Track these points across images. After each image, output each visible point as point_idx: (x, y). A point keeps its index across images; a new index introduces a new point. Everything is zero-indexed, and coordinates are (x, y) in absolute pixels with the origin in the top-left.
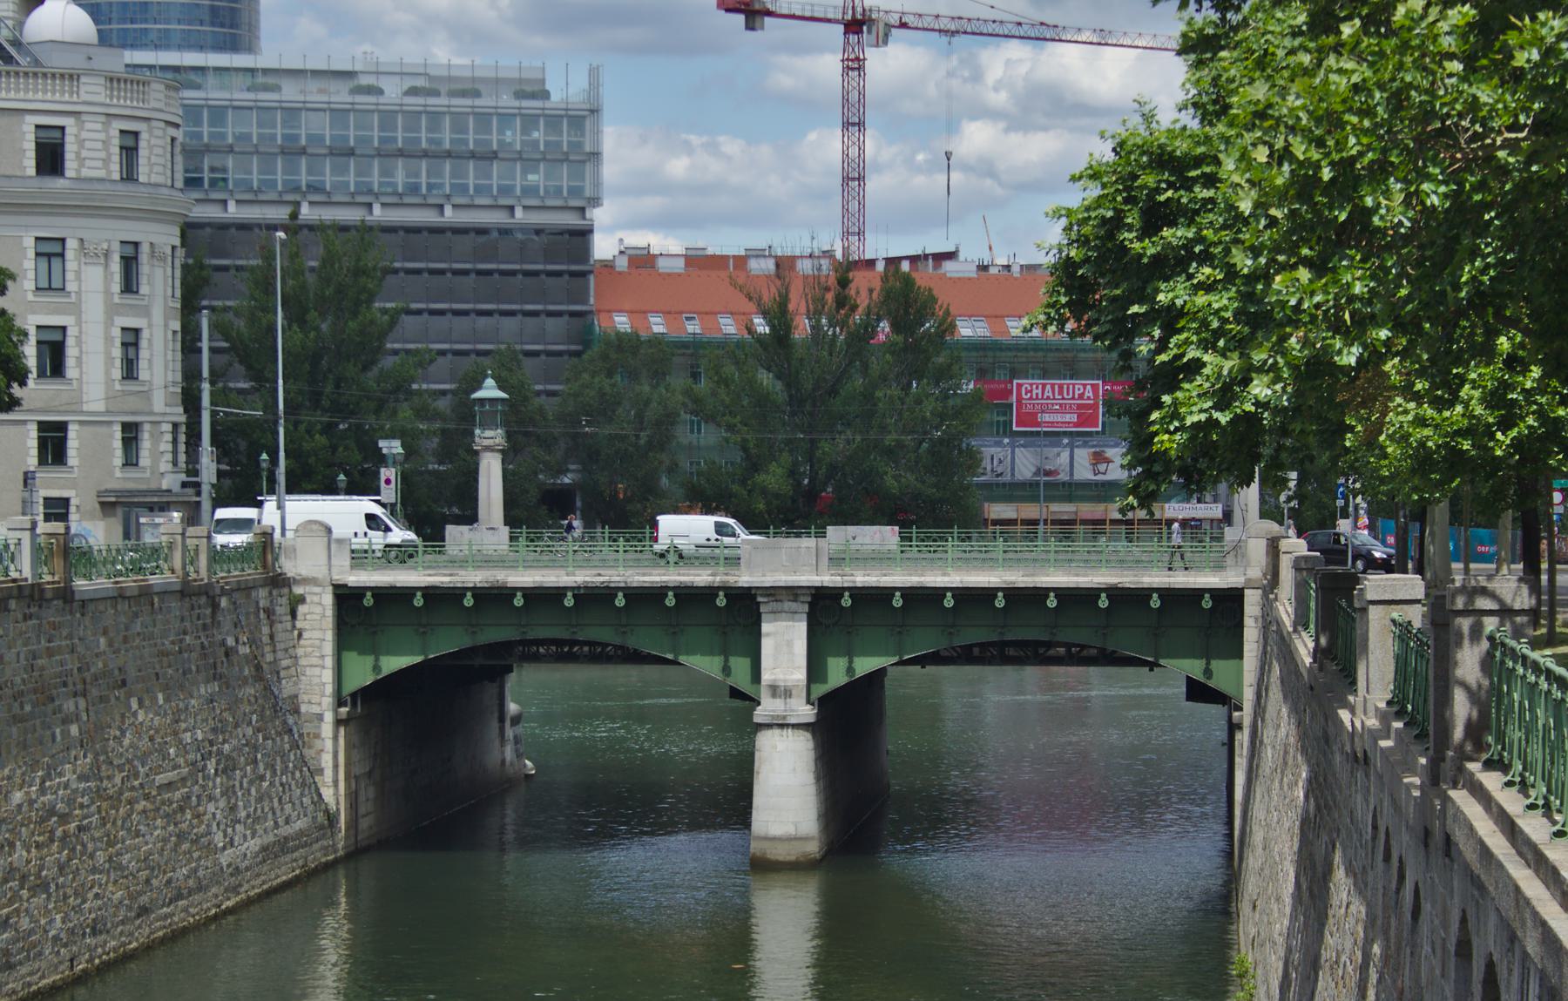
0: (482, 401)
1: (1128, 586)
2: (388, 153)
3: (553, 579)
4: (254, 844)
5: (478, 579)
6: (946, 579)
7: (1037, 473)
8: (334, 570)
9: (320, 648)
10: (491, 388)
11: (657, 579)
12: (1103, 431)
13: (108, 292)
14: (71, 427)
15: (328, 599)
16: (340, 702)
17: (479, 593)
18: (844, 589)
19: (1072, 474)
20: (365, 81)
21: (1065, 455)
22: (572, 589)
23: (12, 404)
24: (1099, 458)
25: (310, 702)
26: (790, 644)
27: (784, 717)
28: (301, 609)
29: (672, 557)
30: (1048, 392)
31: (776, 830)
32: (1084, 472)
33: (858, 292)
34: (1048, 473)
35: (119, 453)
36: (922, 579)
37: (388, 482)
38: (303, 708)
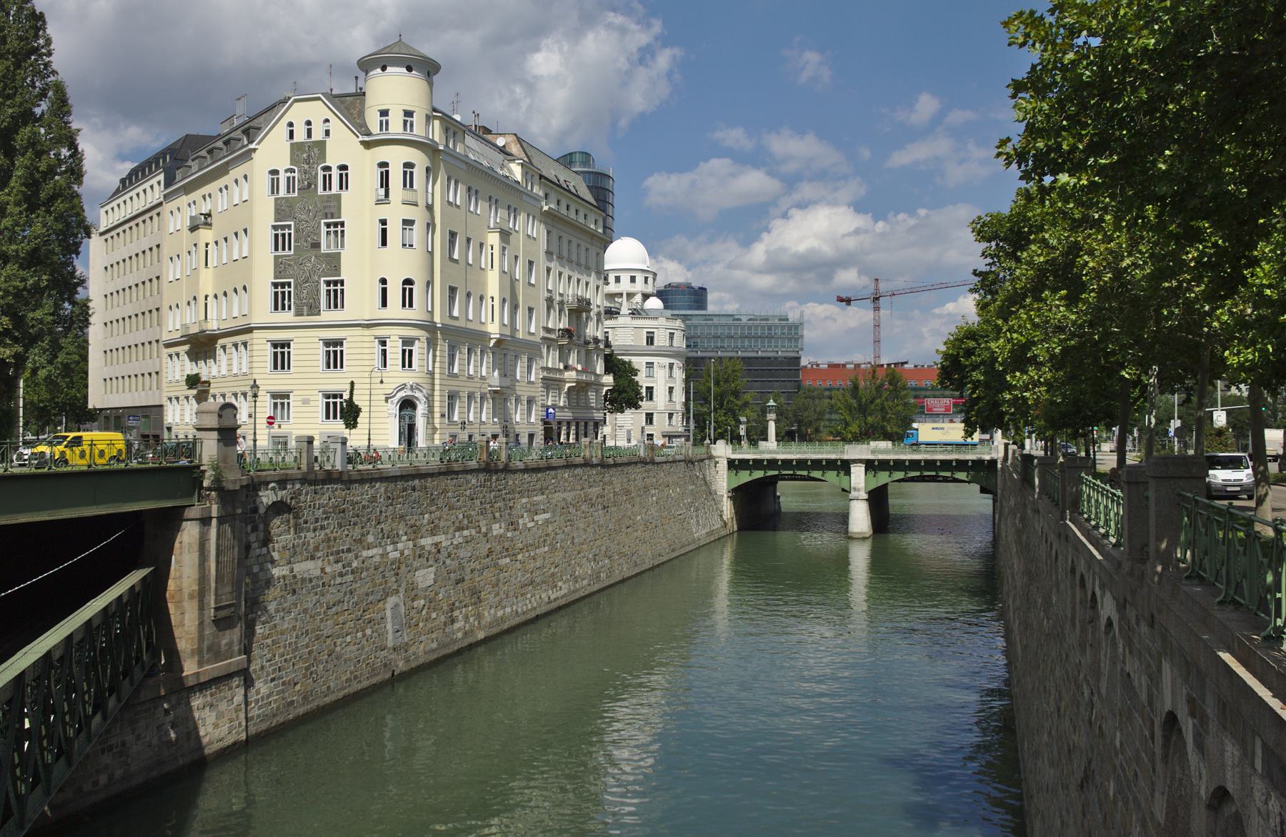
0: (769, 406)
2: (743, 337)
15: (725, 462)
20: (736, 317)
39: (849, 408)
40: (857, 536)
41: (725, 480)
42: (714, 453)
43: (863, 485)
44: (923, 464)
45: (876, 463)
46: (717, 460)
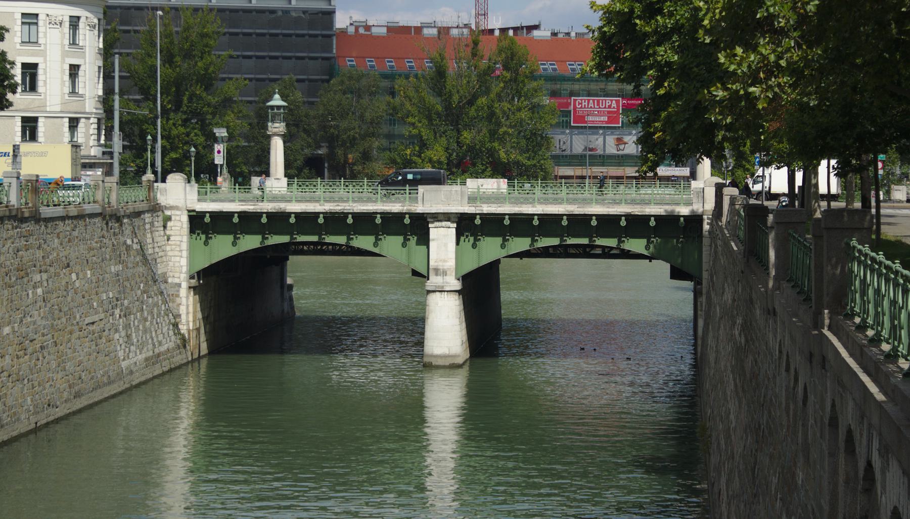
0: (272, 107)
1: (637, 213)
3: (312, 208)
6: (534, 209)
7: (585, 149)
8: (188, 202)
9: (180, 246)
11: (371, 208)
12: (622, 127)
13: (63, 45)
14: (40, 120)
15: (185, 219)
16: (192, 277)
18: (476, 214)
19: (604, 151)
21: (601, 140)
24: (620, 141)
25: (173, 277)
26: (446, 245)
27: (443, 287)
28: (169, 224)
30: (591, 105)
31: (437, 351)
32: (611, 149)
34: (591, 150)
36: (521, 209)
40: (440, 362)
41: (185, 254)
42: (162, 200)
46: (168, 213)
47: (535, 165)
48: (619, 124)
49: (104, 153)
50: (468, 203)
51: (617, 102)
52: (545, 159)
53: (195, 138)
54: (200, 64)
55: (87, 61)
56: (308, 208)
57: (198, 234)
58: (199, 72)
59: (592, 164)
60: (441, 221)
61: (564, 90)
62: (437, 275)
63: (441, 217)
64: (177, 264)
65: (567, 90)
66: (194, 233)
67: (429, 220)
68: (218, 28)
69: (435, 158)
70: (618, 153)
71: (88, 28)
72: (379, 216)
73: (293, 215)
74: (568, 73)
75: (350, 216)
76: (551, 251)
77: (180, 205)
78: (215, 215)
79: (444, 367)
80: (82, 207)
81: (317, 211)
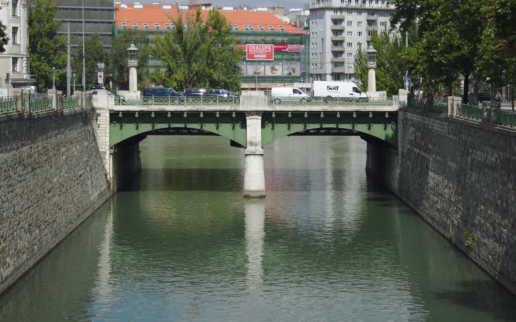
0: (130, 51)
1: (362, 110)
3: (180, 108)
4: (96, 194)
5: (156, 108)
6: (305, 108)
7: (255, 73)
8: (109, 105)
9: (105, 130)
10: (372, 48)
11: (213, 108)
12: (274, 61)
15: (108, 115)
16: (111, 148)
17: (156, 113)
18: (273, 111)
19: (265, 74)
21: (263, 68)
22: (186, 111)
23: (3, 50)
24: (273, 69)
25: (102, 148)
26: (256, 129)
27: (255, 152)
28: (99, 118)
29: (278, 101)
30: (257, 48)
31: (253, 188)
32: (269, 73)
33: (203, 17)
34: (258, 73)
35: (11, 67)
36: (297, 108)
37: (100, 76)
38: (100, 150)
39: (174, 54)
40: (254, 195)
41: (108, 135)
42: (95, 104)
43: (259, 139)
44: (322, 116)
45: (274, 115)
46: (98, 112)
47: (232, 82)
48: (272, 59)
49: (31, 77)
50: (268, 105)
51: (271, 47)
52: (237, 79)
53: (45, 68)
54: (47, 26)
55: (22, 25)
56: (178, 108)
57: (115, 124)
58: (46, 31)
59: (259, 82)
60: (253, 115)
61: (242, 40)
62: (251, 145)
63: (253, 113)
64: (104, 141)
65: (243, 40)
66: (112, 123)
67: (246, 115)
68: (56, 5)
69: (178, 79)
70: (272, 75)
71: (22, 6)
72: (218, 113)
73: (169, 113)
74: (244, 31)
75: (202, 113)
76: (159, 131)
77: (105, 107)
78: (125, 113)
79: (257, 197)
80: (74, 109)
81: (183, 110)
